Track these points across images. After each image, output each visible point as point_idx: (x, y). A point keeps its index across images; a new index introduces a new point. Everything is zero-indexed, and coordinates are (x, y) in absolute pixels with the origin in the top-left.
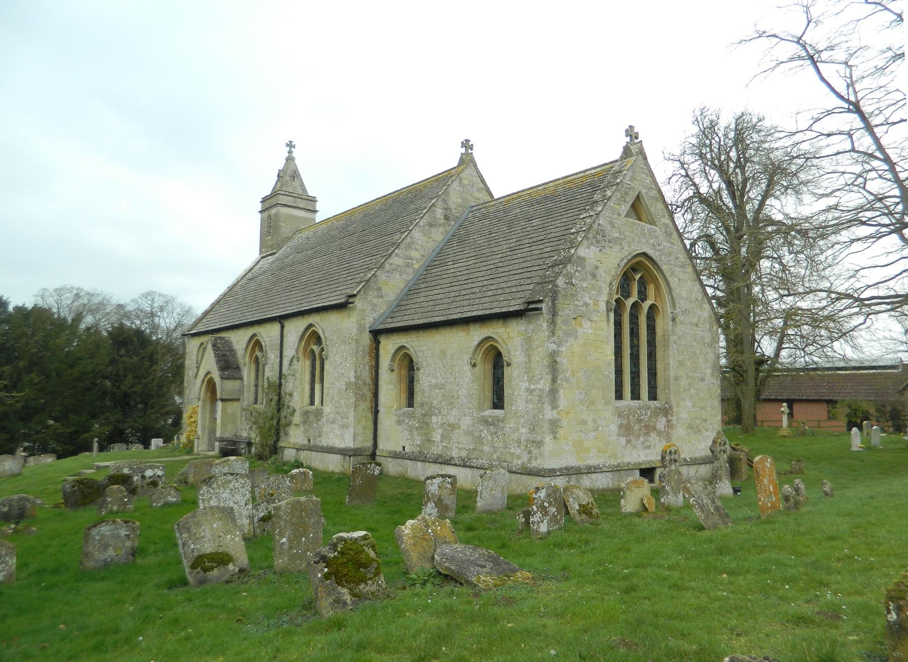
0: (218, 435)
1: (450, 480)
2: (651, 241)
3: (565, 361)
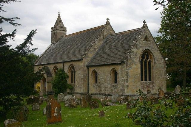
0: (47, 91)
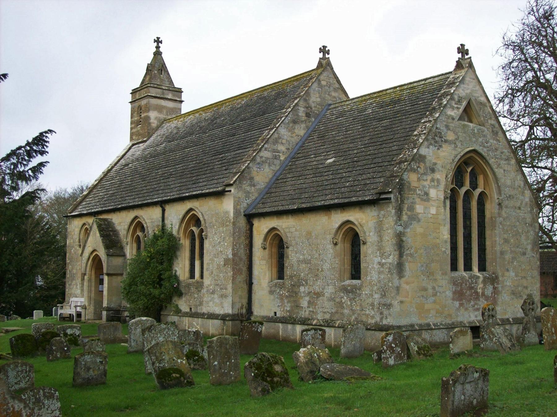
0: (105, 304)
1: (320, 333)
2: (480, 140)
3: (410, 240)
